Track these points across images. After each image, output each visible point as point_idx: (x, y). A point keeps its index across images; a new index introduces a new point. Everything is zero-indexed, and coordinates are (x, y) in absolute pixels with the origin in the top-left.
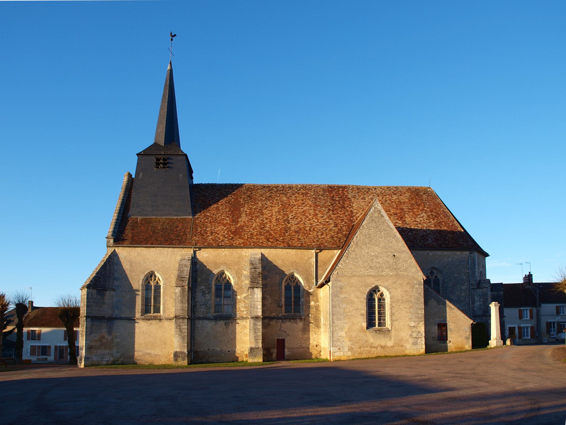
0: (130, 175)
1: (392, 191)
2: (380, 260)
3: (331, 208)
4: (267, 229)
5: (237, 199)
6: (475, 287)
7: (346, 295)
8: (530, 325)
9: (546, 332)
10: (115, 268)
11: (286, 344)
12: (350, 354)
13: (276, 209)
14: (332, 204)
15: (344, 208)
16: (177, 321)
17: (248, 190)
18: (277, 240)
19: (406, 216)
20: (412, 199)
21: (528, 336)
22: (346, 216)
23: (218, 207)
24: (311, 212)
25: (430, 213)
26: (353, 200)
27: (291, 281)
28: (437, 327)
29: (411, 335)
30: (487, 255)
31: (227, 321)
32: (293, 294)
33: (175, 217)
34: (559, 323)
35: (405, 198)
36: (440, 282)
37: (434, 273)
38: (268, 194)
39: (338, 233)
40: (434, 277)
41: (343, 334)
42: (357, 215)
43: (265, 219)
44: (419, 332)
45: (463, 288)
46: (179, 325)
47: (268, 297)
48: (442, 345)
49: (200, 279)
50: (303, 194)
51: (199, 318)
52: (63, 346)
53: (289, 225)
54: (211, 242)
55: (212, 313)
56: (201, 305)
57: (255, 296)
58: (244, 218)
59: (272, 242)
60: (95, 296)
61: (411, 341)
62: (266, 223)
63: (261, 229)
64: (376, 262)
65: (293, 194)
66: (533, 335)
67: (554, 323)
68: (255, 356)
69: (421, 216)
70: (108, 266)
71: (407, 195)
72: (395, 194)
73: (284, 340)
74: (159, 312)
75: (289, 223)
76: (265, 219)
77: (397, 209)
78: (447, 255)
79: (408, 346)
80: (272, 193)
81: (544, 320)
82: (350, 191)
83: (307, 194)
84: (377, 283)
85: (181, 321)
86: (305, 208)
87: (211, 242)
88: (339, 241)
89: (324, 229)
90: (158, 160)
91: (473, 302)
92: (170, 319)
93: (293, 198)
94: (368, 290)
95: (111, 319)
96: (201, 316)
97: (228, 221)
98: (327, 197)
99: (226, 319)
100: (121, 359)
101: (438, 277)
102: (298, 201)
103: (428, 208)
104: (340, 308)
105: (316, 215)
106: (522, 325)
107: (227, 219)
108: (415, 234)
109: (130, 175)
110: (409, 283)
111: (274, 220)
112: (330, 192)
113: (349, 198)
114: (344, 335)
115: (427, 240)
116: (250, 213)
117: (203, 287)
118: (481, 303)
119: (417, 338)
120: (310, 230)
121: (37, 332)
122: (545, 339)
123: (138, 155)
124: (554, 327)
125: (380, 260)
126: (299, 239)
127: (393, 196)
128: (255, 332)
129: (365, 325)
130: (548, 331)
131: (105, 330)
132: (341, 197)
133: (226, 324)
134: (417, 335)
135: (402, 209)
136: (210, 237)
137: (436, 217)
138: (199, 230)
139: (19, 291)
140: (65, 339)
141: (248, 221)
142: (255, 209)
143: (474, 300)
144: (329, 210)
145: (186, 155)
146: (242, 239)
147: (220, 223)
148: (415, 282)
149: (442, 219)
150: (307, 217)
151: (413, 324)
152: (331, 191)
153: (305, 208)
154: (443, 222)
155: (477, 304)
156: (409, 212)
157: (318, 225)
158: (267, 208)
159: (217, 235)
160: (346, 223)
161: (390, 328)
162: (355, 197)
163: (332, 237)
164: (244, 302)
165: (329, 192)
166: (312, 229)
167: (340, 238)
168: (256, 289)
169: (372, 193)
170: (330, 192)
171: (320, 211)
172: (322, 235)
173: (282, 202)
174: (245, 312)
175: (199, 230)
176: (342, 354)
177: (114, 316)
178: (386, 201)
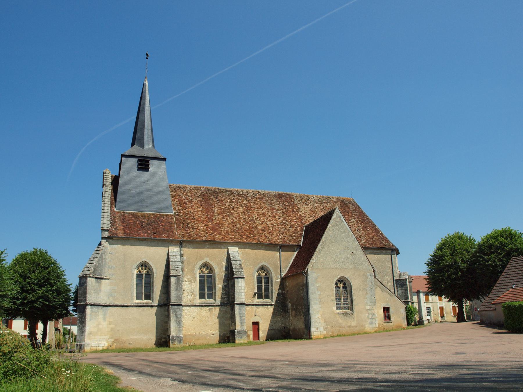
2: (343, 256)
12: (325, 333)
13: (241, 210)
23: (193, 206)
29: (368, 317)
33: (158, 213)
42: (305, 219)
43: (234, 219)
44: (373, 314)
46: (175, 311)
50: (259, 198)
57: (240, 285)
60: (94, 284)
70: (104, 255)
74: (145, 299)
79: (367, 325)
83: (262, 198)
86: (264, 211)
96: (189, 303)
97: (204, 218)
110: (364, 275)
115: (361, 240)
116: (221, 213)
117: (189, 277)
122: (231, 341)
125: (343, 256)
128: (240, 317)
129: (334, 308)
133: (210, 310)
136: (193, 233)
140: (25, 328)
142: (224, 209)
144: (283, 213)
146: (220, 234)
153: (264, 211)
163: (291, 236)
170: (281, 198)
172: (283, 234)
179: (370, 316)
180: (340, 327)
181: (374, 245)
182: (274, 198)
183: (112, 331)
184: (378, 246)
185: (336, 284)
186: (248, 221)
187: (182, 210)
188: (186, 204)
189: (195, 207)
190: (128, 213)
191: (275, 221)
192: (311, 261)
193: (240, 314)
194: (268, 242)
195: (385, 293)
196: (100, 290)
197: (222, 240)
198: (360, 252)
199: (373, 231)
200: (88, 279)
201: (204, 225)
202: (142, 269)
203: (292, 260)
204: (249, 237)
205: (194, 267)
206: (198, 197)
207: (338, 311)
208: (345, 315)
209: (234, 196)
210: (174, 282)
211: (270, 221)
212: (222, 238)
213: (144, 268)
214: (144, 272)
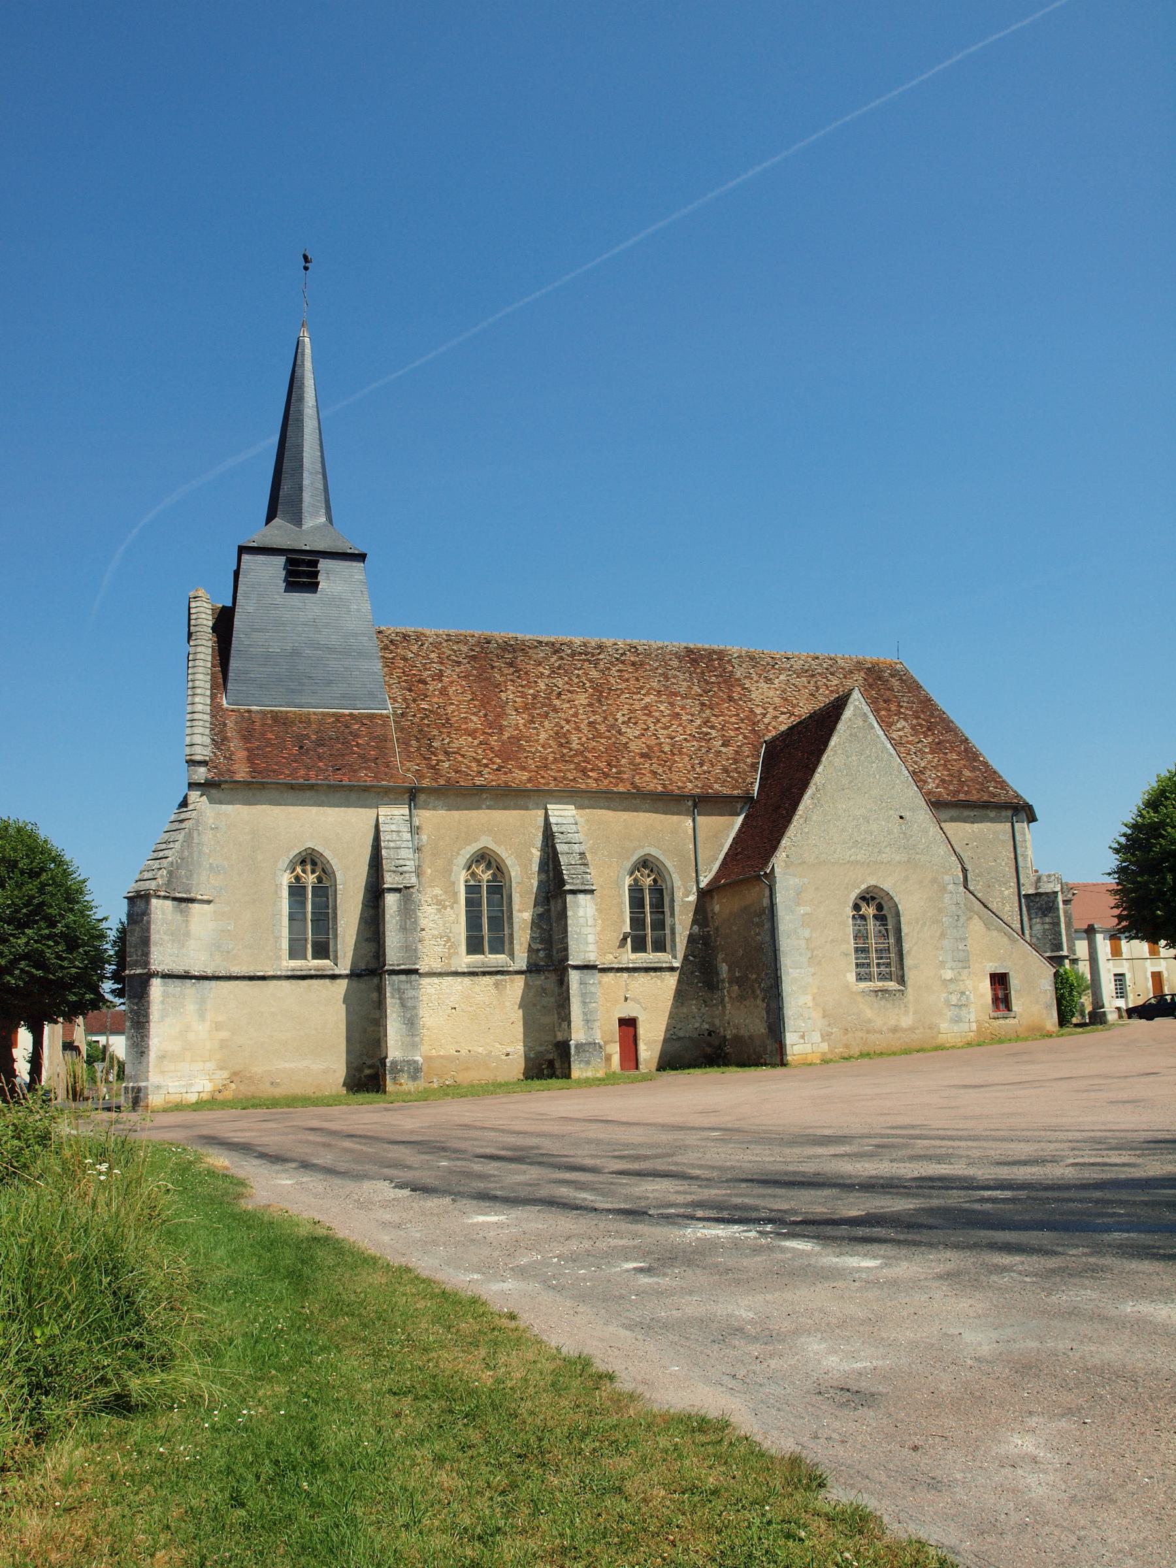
3: (705, 699)
12: (824, 1047)
13: (582, 699)
18: (606, 775)
25: (915, 722)
42: (766, 721)
43: (563, 723)
44: (963, 993)
49: (429, 871)
50: (633, 664)
57: (581, 913)
58: (515, 720)
63: (561, 745)
69: (899, 726)
72: (832, 674)
74: (314, 958)
76: (563, 723)
79: (944, 1026)
86: (647, 700)
89: (704, 750)
96: (437, 966)
97: (476, 722)
104: (798, 938)
113: (739, 680)
114: (810, 1004)
117: (437, 891)
121: (654, 917)
129: (851, 977)
134: (959, 1000)
139: (89, 885)
142: (535, 697)
144: (703, 704)
150: (658, 721)
153: (647, 700)
162: (749, 677)
163: (725, 770)
170: (694, 662)
172: (701, 765)
174: (542, 954)
176: (808, 1048)
178: (818, 688)
179: (954, 999)
181: (962, 796)
182: (675, 663)
184: (974, 798)
186: (602, 728)
187: (414, 701)
189: (451, 691)
190: (261, 712)
193: (583, 995)
194: (660, 788)
195: (995, 933)
196: (187, 934)
198: (923, 815)
201: (476, 742)
203: (730, 841)
204: (606, 775)
209: (562, 658)
212: (530, 780)
213: (309, 868)
214: (310, 879)
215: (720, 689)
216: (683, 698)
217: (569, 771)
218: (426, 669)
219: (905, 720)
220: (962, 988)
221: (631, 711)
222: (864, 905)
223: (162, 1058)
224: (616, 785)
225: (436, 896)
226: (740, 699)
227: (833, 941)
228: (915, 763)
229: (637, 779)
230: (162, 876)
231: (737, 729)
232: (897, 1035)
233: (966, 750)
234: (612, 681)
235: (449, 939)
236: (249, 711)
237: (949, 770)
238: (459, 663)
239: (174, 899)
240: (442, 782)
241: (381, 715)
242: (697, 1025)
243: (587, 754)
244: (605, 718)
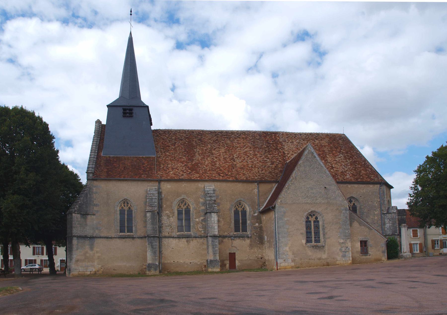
0: (98, 122)
1: (314, 136)
4: (217, 165)
5: (190, 142)
6: (385, 212)
7: (288, 218)
8: (419, 242)
9: (431, 247)
10: (95, 197)
11: (236, 257)
12: (293, 264)
13: (223, 150)
14: (268, 147)
15: (278, 150)
16: (149, 239)
17: (198, 135)
18: (227, 175)
19: (328, 156)
20: (331, 143)
21: (417, 251)
22: (280, 156)
23: (175, 148)
24: (251, 152)
26: (284, 143)
27: (239, 207)
28: (359, 243)
29: (341, 250)
30: (392, 187)
31: (188, 239)
32: (240, 218)
33: (141, 156)
34: (441, 241)
35: (324, 143)
36: (357, 208)
37: (352, 201)
38: (215, 138)
39: (275, 169)
40: (352, 204)
41: (287, 249)
42: (289, 156)
43: (215, 158)
44: (347, 247)
45: (376, 213)
47: (221, 219)
48: (364, 257)
49: (165, 206)
50: (243, 138)
51: (165, 237)
52: (32, 260)
53: (235, 163)
54: (173, 176)
55: (176, 233)
56: (166, 226)
57: (213, 219)
58: (198, 157)
59: (223, 176)
61: (341, 254)
62: (216, 161)
63: (212, 165)
64: (311, 193)
65: (236, 138)
66: (421, 251)
67: (438, 240)
68: (214, 267)
70: (89, 195)
71: (327, 139)
72: (316, 139)
73: (235, 253)
75: (234, 161)
77: (320, 151)
78: (362, 187)
79: (339, 258)
80: (218, 137)
81: (430, 238)
82: (281, 136)
83: (246, 138)
84: (313, 209)
85: (152, 239)
86: (246, 150)
87: (173, 176)
88: (277, 176)
89: (263, 166)
90: (124, 110)
91: (384, 224)
92: (141, 238)
93: (236, 141)
94: (306, 214)
95: (92, 238)
96: (167, 235)
97: (185, 159)
98: (263, 141)
99: (187, 237)
100: (102, 270)
101: (356, 204)
102: (240, 144)
103: (344, 150)
105: (255, 155)
106: (412, 242)
107: (184, 157)
108: (336, 171)
109: (98, 122)
110: (337, 209)
111: (222, 159)
112: (265, 137)
113: (281, 142)
115: (346, 175)
116: (202, 154)
117: (167, 212)
118: (391, 225)
119: (346, 252)
120: (252, 167)
123: (108, 106)
124: (438, 244)
126: (244, 174)
127: (316, 140)
128: (213, 248)
129: (304, 241)
130: (433, 247)
131: (88, 246)
132: (274, 141)
133: (187, 241)
134: (346, 249)
135: (324, 151)
136: (171, 172)
137: (351, 157)
138: (162, 166)
141: (201, 159)
142: (206, 150)
143: (385, 222)
144: (266, 151)
145: (148, 107)
146: (198, 173)
147: (178, 161)
148: (342, 208)
149: (356, 159)
150: (249, 157)
151: (342, 241)
152: (266, 136)
153: (246, 150)
154: (357, 161)
155: (387, 225)
156: (329, 153)
157: (258, 163)
158: (215, 149)
159: (177, 170)
160: (280, 161)
161: (324, 245)
164: (202, 223)
165: (264, 137)
166: (253, 167)
167: (277, 173)
168: (213, 214)
169: (299, 138)
171: (258, 152)
172: (262, 171)
173: (227, 144)
174: (203, 232)
175: (162, 166)
176: (286, 264)
177: (94, 235)
179: (343, 249)
180: (310, 259)
181: (359, 180)
182: (258, 137)
183: (98, 258)
184: (364, 180)
185: (308, 218)
186: (228, 160)
187: (164, 152)
188: (169, 147)
189: (177, 149)
190: (113, 157)
191: (256, 159)
192: (280, 196)
193: (213, 245)
194: (245, 179)
195: (363, 227)
196: (86, 225)
197: (198, 179)
198: (334, 186)
199: (361, 165)
200: (74, 214)
201: (183, 165)
202: (124, 206)
203: (270, 196)
204: (227, 175)
205: (172, 203)
206: (182, 140)
207: (308, 244)
208: (316, 248)
209: (218, 137)
210: (150, 217)
211: (251, 159)
212: (199, 177)
213: (126, 205)
214: (126, 208)
215: (273, 146)
216: (259, 149)
217: (214, 174)
218: (170, 142)
219: (342, 154)
220: (347, 245)
221: (239, 154)
222: (310, 217)
223: (77, 261)
224: (229, 178)
225: (167, 214)
226: (280, 149)
227: (297, 229)
228: (343, 169)
229: (237, 176)
230: (77, 207)
231: (277, 159)
232: (321, 261)
233: (364, 164)
234: (234, 144)
235: (171, 227)
236: (110, 157)
237: (356, 171)
238: (182, 140)
239: (81, 214)
240: (169, 178)
241: (152, 157)
242: (257, 255)
243: (221, 168)
244: (230, 156)
